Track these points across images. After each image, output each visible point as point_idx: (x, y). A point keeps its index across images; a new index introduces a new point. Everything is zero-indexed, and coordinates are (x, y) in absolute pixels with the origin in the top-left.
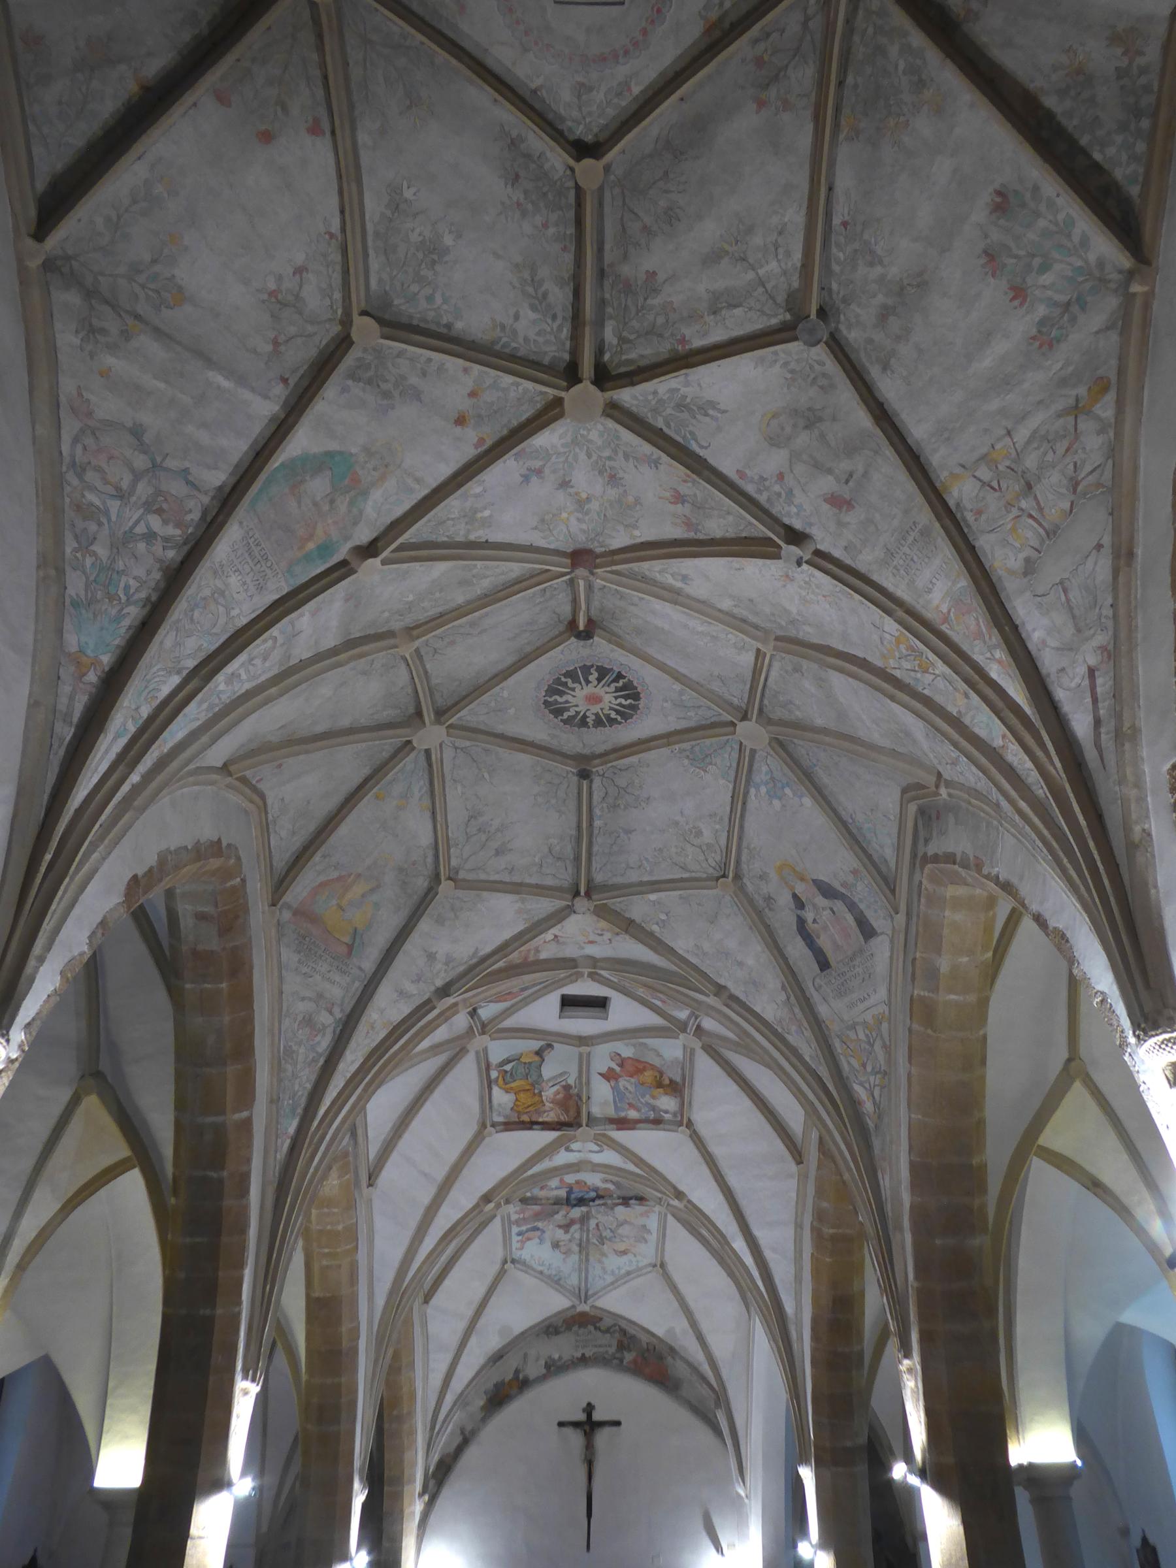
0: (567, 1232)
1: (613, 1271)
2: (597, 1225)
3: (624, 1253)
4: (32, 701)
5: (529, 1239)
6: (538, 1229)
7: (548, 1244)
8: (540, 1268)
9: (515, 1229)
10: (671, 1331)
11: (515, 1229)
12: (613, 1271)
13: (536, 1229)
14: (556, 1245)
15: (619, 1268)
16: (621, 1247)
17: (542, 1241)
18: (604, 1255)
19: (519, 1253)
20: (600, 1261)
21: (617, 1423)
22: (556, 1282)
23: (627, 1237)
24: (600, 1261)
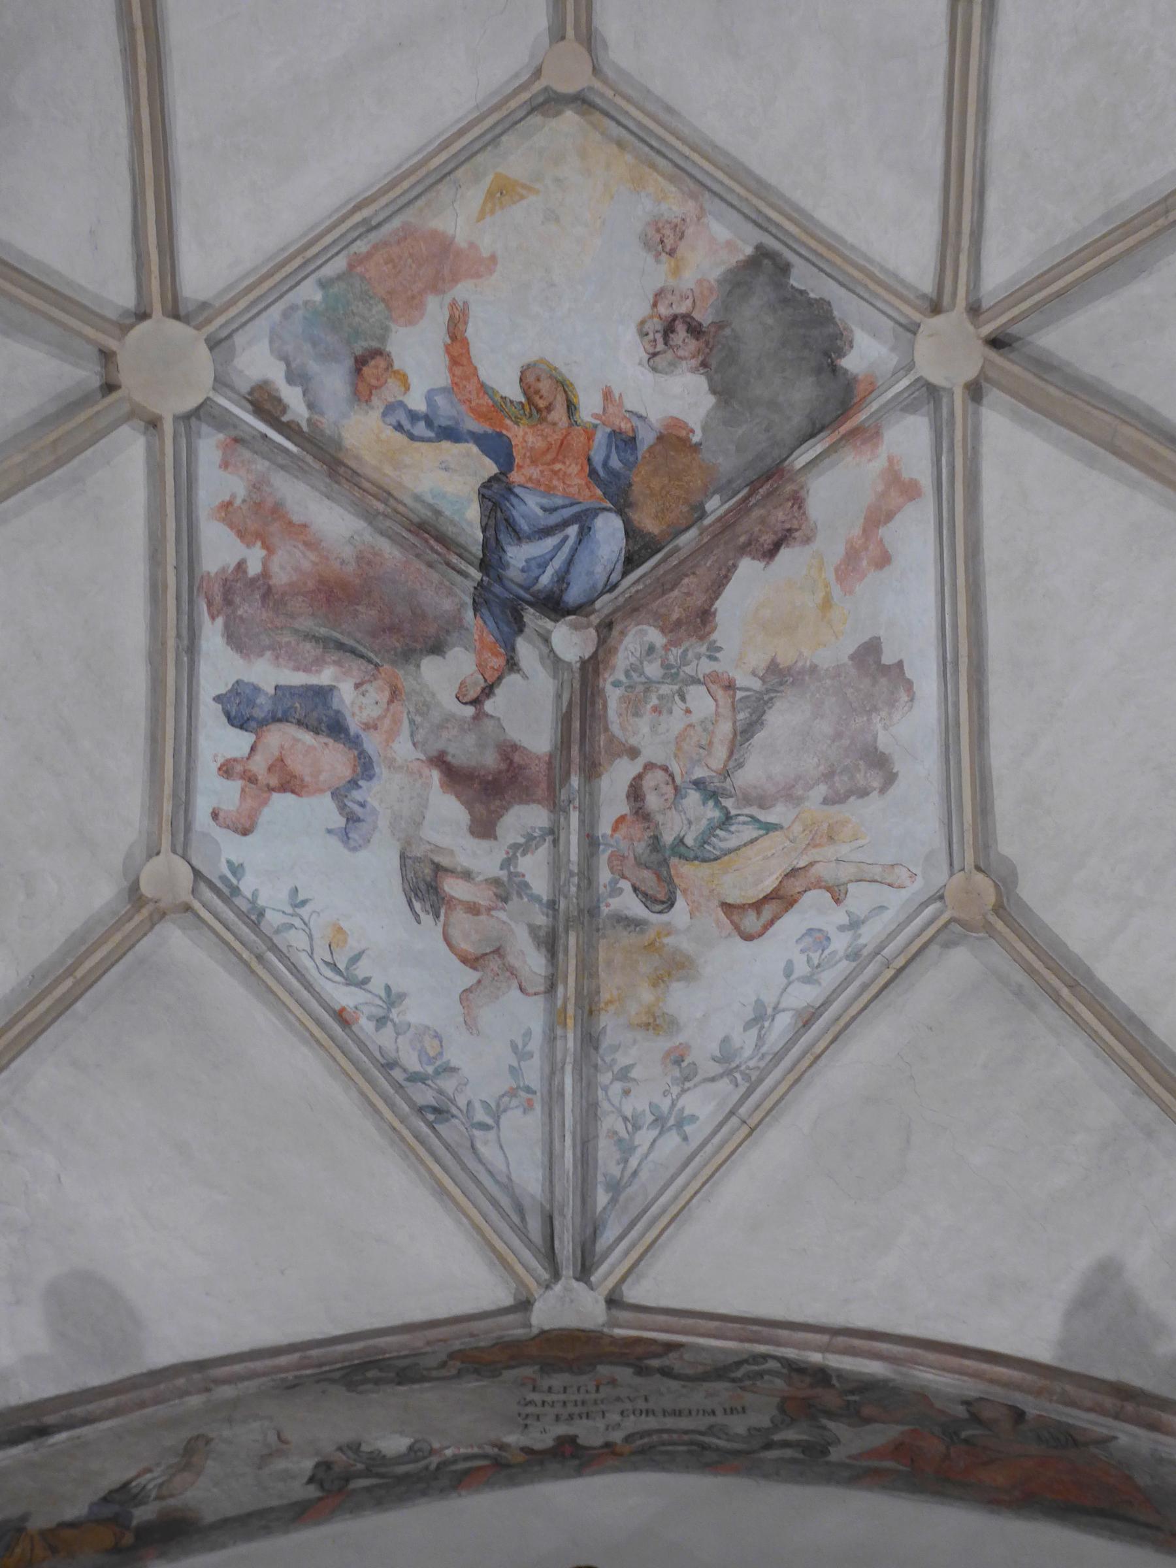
0: (484, 828)
1: (726, 1056)
2: (635, 793)
3: (781, 900)
4: (108, 1511)
5: (290, 784)
6: (336, 728)
7: (380, 862)
8: (344, 997)
9: (220, 666)
10: (1102, 1291)
11: (220, 666)
12: (726, 1056)
13: (318, 714)
14: (426, 885)
15: (760, 1017)
16: (754, 872)
17: (352, 825)
18: (676, 967)
19: (231, 848)
20: (655, 1023)
21: (419, 923)
22: (423, 1115)
23: (789, 794)
24: (655, 1023)
